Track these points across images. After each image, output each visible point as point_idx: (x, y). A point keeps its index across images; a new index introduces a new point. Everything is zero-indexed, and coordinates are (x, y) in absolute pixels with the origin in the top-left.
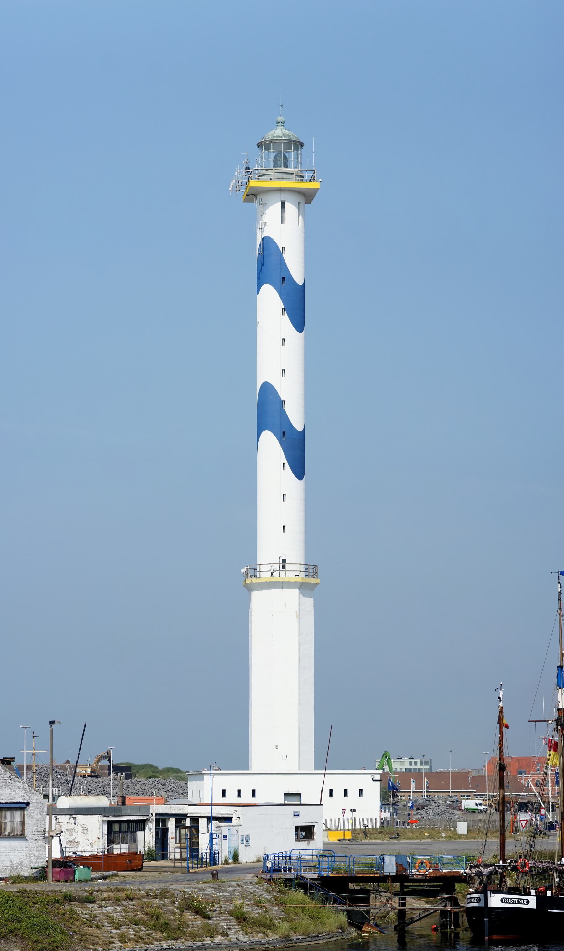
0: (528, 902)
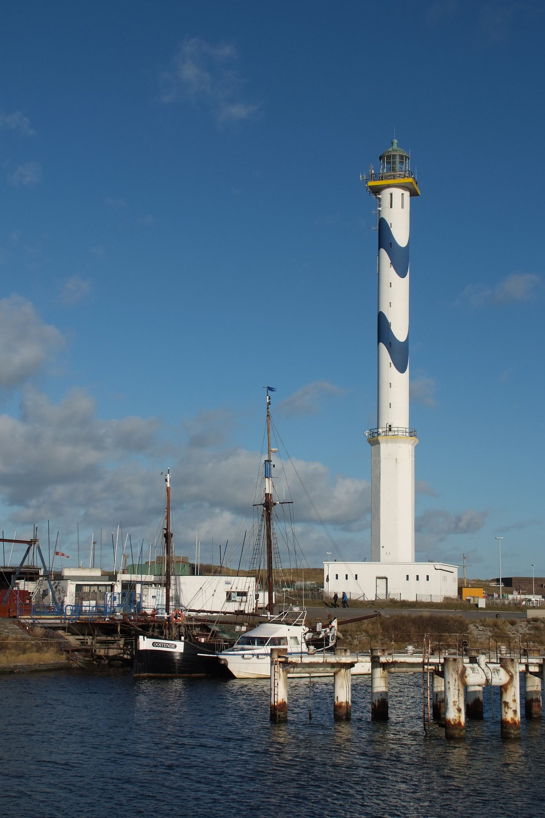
0: (175, 647)
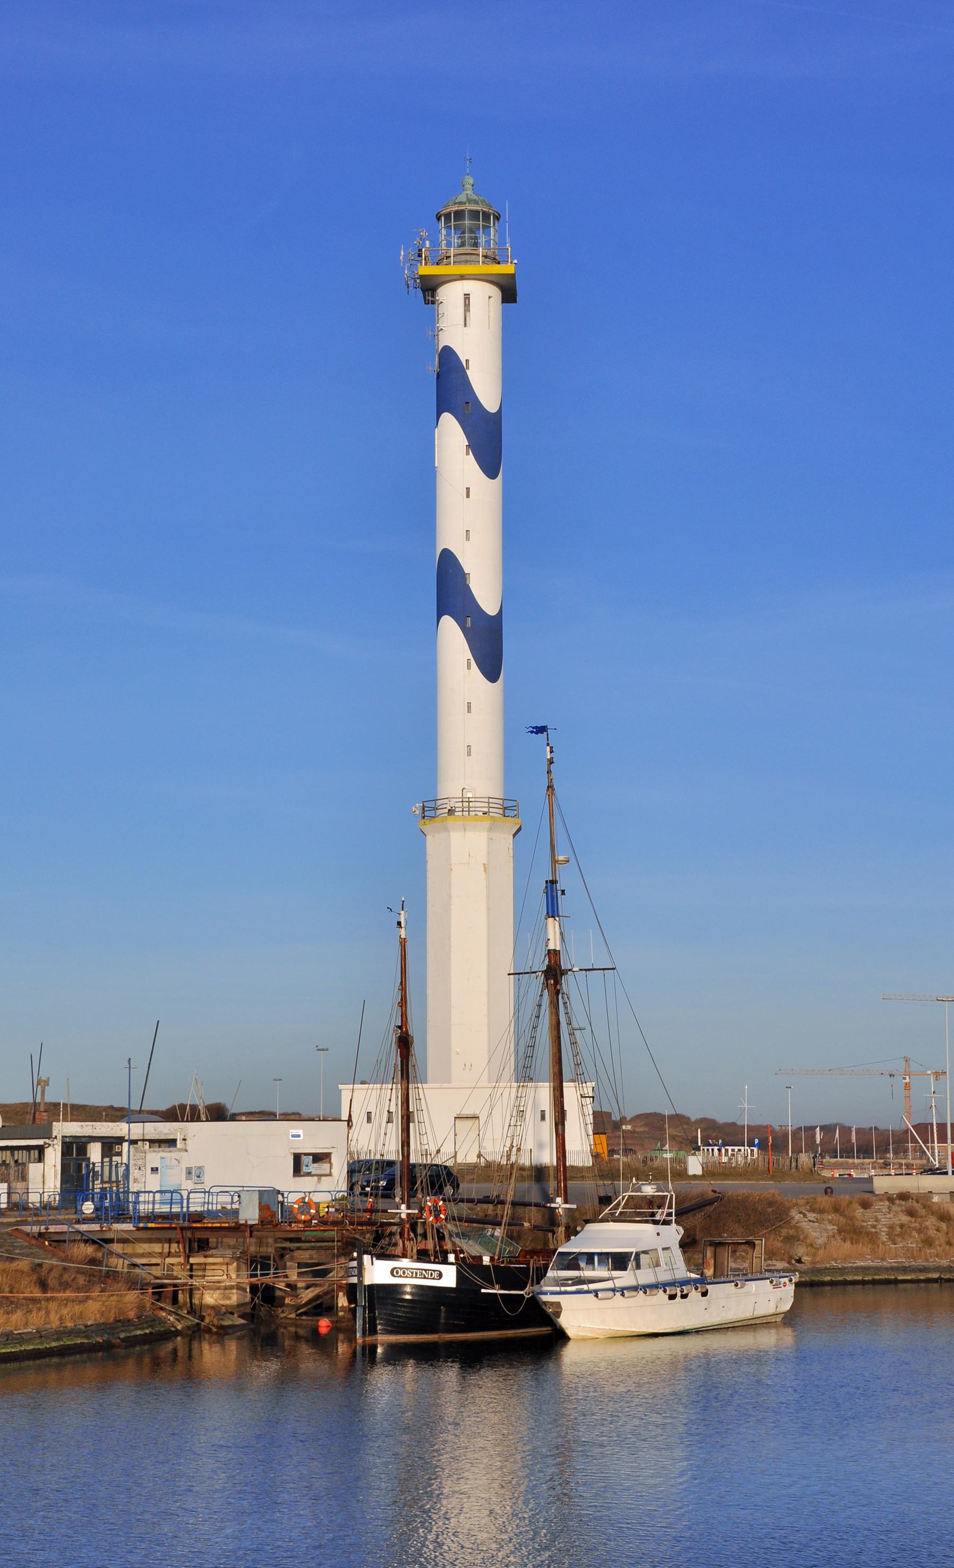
0: (440, 1275)
